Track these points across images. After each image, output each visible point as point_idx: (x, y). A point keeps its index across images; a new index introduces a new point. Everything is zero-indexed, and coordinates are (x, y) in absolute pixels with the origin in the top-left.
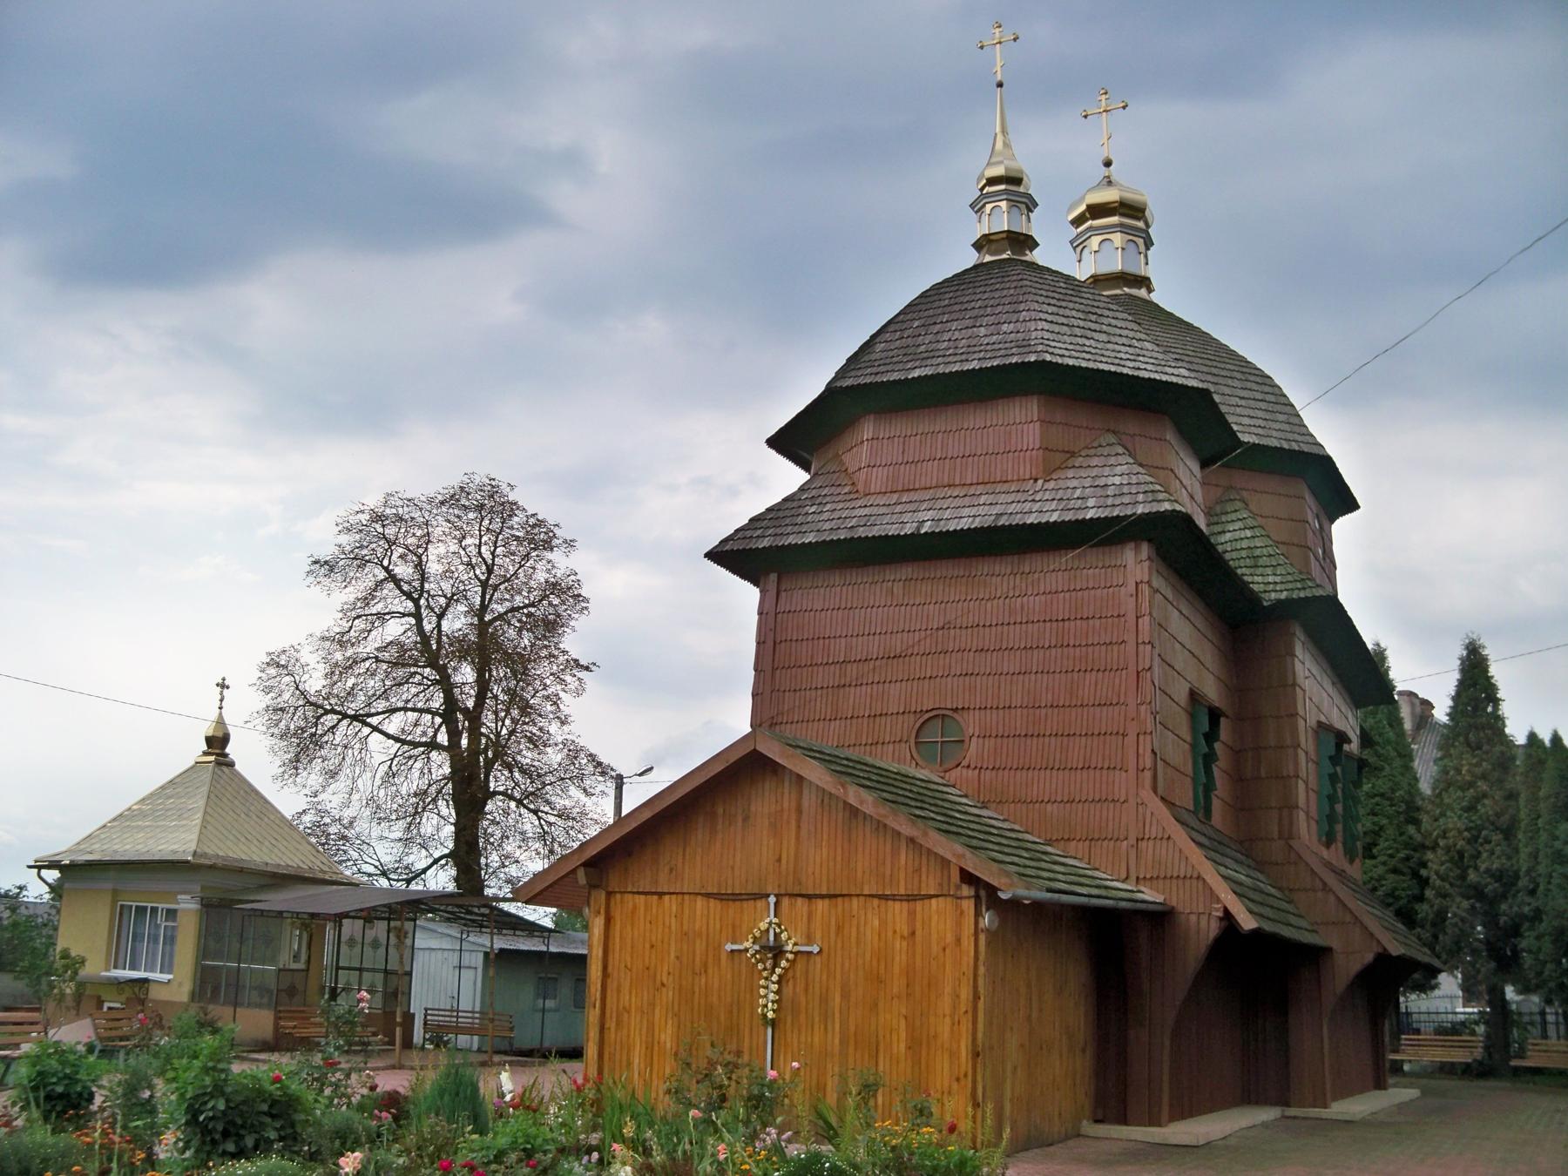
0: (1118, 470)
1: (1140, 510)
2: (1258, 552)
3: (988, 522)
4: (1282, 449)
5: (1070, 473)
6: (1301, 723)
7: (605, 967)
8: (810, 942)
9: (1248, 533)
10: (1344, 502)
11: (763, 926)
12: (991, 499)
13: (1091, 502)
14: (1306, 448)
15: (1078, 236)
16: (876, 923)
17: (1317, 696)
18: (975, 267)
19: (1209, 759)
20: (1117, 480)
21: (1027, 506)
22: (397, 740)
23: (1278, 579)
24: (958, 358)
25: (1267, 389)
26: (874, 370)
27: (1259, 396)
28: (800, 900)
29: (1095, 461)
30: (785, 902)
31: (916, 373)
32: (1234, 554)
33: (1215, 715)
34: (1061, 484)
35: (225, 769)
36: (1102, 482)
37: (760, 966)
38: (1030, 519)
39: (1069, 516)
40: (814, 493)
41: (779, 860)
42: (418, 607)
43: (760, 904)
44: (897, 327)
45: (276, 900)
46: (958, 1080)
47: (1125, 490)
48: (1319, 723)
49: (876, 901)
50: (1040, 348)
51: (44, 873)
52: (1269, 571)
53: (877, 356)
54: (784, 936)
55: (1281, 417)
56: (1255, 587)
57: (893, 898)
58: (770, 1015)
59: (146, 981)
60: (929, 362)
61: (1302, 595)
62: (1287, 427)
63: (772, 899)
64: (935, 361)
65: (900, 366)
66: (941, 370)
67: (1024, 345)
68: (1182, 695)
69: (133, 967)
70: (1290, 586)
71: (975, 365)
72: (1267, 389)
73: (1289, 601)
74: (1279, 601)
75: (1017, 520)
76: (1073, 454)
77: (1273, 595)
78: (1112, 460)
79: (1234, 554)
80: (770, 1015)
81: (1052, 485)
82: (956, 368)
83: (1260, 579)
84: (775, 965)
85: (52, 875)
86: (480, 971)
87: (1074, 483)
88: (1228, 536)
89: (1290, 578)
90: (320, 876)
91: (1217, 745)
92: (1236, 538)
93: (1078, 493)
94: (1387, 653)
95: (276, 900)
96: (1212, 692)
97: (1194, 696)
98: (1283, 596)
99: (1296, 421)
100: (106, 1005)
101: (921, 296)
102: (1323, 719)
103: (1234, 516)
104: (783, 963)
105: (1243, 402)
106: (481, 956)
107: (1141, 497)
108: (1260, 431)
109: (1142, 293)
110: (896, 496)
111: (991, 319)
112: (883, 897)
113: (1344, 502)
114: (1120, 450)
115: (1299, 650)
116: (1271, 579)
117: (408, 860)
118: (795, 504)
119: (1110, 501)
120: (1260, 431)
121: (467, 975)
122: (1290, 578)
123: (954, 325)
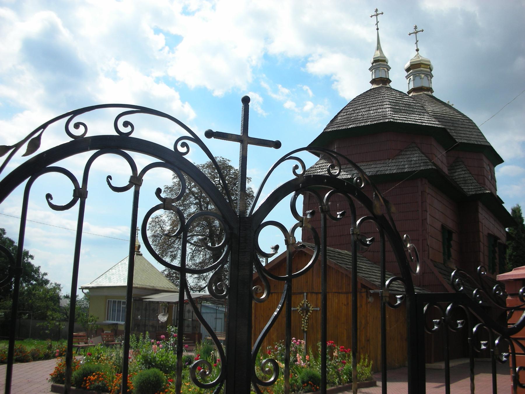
0: (415, 155)
1: (422, 168)
2: (466, 178)
3: (374, 173)
4: (474, 144)
5: (400, 157)
6: (481, 234)
7: (255, 316)
8: (317, 307)
9: (463, 172)
10: (499, 160)
11: (303, 302)
12: (375, 166)
13: (406, 166)
14: (483, 143)
15: (408, 75)
16: (337, 301)
17: (487, 223)
18: (371, 90)
19: (449, 246)
20: (415, 159)
21: (386, 168)
22: (194, 245)
23: (472, 187)
24: (364, 121)
25: (470, 124)
26: (338, 126)
27: (467, 127)
28: (314, 294)
29: (408, 153)
30: (309, 295)
31: (351, 127)
32: (459, 180)
33: (450, 233)
34: (398, 160)
35: (139, 256)
36: (410, 159)
37: (302, 315)
38: (387, 172)
39: (399, 171)
40: (320, 165)
41: (307, 282)
42: (200, 201)
43: (302, 295)
44: (345, 111)
45: (156, 298)
46: (362, 348)
47: (417, 162)
48: (489, 234)
49: (336, 294)
50: (389, 117)
51: (84, 291)
52: (470, 185)
53: (338, 121)
54: (309, 305)
55: (475, 133)
56: (465, 190)
57: (342, 293)
58: (305, 329)
59: (117, 324)
60: (354, 123)
61: (480, 192)
62: (477, 137)
63: (305, 294)
64: (356, 122)
65: (346, 124)
66: (358, 125)
67: (385, 116)
68: (438, 225)
69: (113, 319)
70: (476, 189)
71: (369, 123)
72: (470, 124)
73: (476, 195)
74: (473, 195)
75: (383, 173)
76: (401, 151)
77: (471, 193)
78: (414, 152)
79: (459, 180)
80: (305, 329)
81: (394, 161)
82: (362, 124)
83: (466, 187)
84: (307, 314)
85: (86, 291)
86: (223, 319)
87: (400, 160)
88: (457, 174)
89: (476, 187)
90: (171, 290)
91: (452, 242)
92: (460, 174)
93: (402, 163)
94: (521, 208)
95: (156, 298)
96: (450, 224)
97: (443, 227)
98: (474, 193)
99: (480, 134)
100: (105, 332)
101: (353, 100)
102: (490, 232)
103: (459, 167)
104: (309, 314)
105: (462, 129)
106: (223, 315)
107: (422, 164)
108: (467, 138)
109: (430, 93)
110: (345, 166)
111: (375, 108)
112: (339, 293)
113: (499, 160)
114: (416, 149)
115: (480, 210)
116: (470, 187)
117: (200, 284)
118: (314, 169)
119: (412, 166)
120: (467, 138)
121: (219, 321)
122: (476, 187)
123: (363, 110)
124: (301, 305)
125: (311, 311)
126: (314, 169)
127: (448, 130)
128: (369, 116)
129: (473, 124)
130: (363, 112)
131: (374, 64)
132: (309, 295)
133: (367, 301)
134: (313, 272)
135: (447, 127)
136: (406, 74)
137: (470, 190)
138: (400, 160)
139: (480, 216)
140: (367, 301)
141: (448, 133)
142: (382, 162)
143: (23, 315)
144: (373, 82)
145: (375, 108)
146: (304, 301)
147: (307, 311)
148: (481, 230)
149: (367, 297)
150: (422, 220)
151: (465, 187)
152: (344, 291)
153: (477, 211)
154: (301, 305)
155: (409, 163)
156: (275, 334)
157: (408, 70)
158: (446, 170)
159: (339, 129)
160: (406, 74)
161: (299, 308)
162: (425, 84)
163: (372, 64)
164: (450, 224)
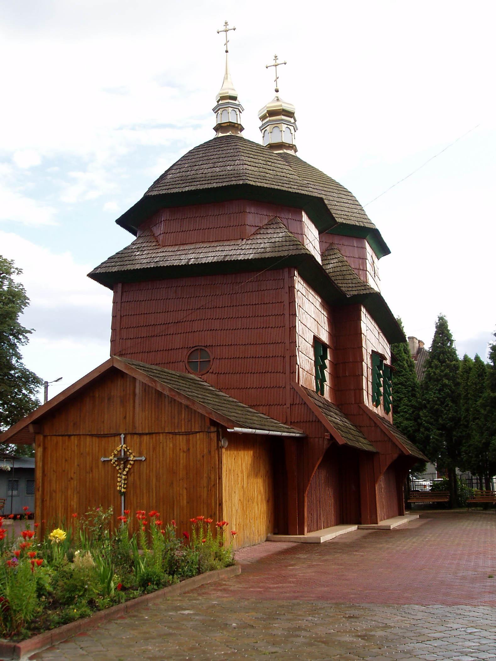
3: (220, 259)
5: (258, 236)
11: (119, 449)
16: (171, 445)
19: (324, 367)
25: (349, 198)
26: (167, 187)
30: (129, 437)
34: (255, 241)
38: (240, 258)
39: (257, 256)
41: (125, 418)
43: (117, 438)
47: (284, 243)
49: (171, 436)
52: (350, 281)
56: (343, 289)
60: (193, 184)
63: (122, 436)
64: (195, 183)
65: (179, 186)
72: (349, 198)
75: (234, 258)
78: (278, 231)
80: (123, 490)
81: (249, 242)
84: (125, 467)
87: (259, 241)
96: (325, 337)
104: (129, 466)
109: (291, 152)
110: (177, 247)
111: (221, 164)
112: (175, 434)
116: (351, 285)
118: (130, 251)
119: (277, 249)
124: (116, 452)
125: (132, 462)
126: (130, 251)
127: (326, 202)
128: (212, 176)
129: (353, 199)
130: (206, 169)
131: (220, 102)
132: (129, 437)
133: (218, 444)
134: (134, 402)
135: (324, 197)
136: (260, 123)
137: (350, 289)
138: (259, 241)
139: (363, 326)
140: (218, 444)
141: (325, 205)
142: (232, 243)
143: (384, 362)
144: (218, 128)
145: (221, 164)
146: (121, 446)
147: (126, 461)
148: (364, 345)
149: (218, 440)
150: (290, 328)
151: (344, 285)
152: (183, 431)
153: (359, 319)
154: (116, 452)
155: (272, 245)
156: (75, 500)
157: (263, 118)
158: (319, 259)
159: (169, 191)
160: (260, 123)
161: (111, 458)
162: (286, 139)
163: (218, 102)
164: (325, 337)
